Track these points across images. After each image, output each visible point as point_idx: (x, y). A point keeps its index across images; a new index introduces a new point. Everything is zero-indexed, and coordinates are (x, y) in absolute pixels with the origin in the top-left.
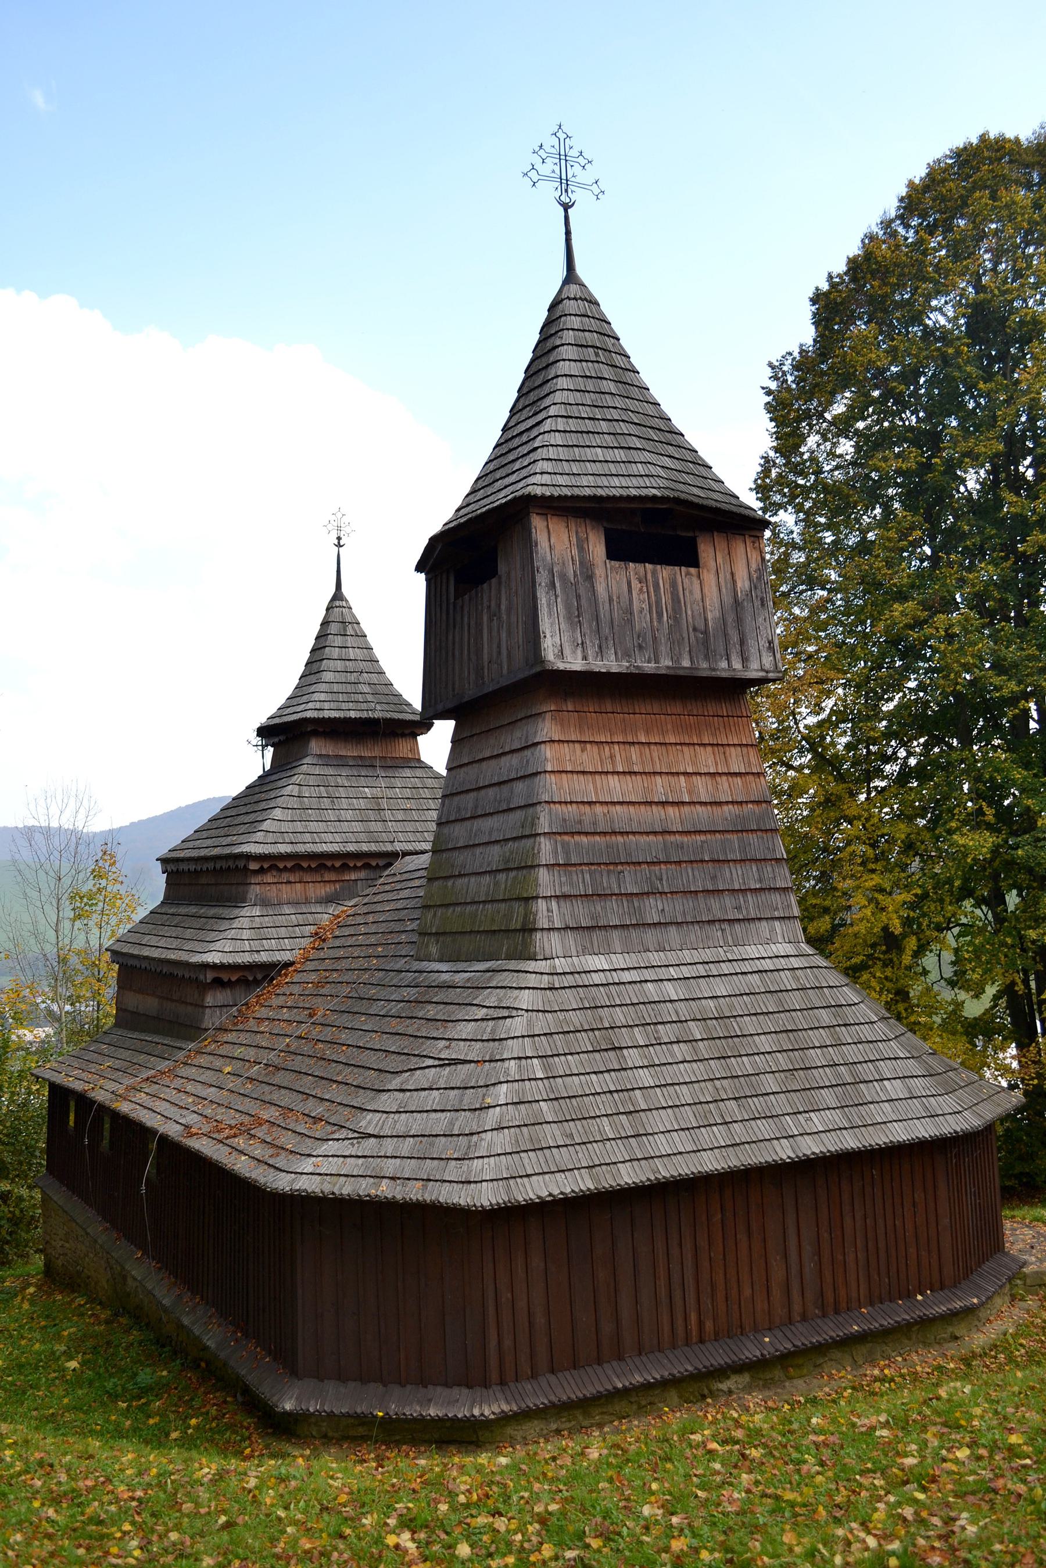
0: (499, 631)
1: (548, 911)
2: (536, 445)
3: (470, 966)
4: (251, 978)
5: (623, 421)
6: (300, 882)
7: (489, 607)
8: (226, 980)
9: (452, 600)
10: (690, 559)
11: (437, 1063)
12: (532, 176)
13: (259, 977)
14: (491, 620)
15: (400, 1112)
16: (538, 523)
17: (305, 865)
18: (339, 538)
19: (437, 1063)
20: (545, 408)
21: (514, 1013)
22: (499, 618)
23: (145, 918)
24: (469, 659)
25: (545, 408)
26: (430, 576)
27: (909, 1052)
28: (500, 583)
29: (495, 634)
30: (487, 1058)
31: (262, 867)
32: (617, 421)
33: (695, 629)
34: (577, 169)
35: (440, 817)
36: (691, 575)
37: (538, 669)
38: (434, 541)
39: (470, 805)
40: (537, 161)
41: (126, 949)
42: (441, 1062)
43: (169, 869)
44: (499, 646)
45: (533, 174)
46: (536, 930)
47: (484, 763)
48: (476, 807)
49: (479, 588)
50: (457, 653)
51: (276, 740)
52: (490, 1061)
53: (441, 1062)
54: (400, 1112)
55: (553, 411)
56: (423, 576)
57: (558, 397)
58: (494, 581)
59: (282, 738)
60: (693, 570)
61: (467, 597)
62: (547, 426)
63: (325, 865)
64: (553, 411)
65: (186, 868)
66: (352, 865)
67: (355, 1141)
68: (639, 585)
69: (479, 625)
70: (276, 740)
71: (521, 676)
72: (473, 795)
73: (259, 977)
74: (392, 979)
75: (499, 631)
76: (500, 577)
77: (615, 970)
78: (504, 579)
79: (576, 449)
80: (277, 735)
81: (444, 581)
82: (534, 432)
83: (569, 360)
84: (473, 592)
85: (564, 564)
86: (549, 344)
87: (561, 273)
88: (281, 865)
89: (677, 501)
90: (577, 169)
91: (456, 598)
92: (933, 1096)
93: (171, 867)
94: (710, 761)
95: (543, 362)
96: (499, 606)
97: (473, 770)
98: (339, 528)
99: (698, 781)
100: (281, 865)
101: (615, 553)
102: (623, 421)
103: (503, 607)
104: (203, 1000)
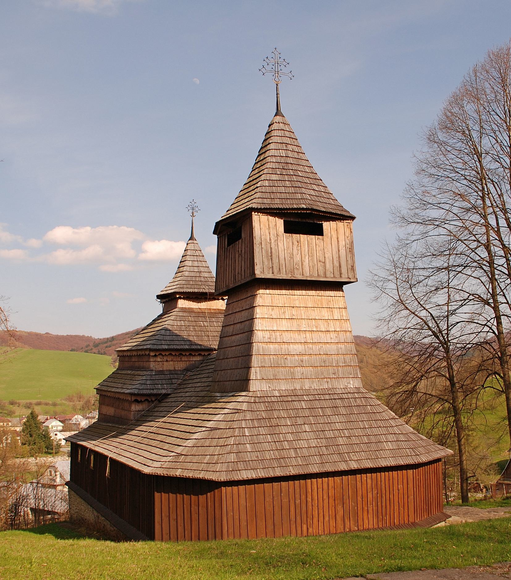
0: (241, 262)
1: (255, 373)
2: (258, 186)
3: (229, 394)
4: (150, 400)
5: (294, 175)
6: (172, 361)
7: (238, 251)
8: (140, 400)
9: (226, 247)
10: (318, 231)
11: (209, 429)
12: (262, 71)
13: (153, 399)
14: (239, 257)
15: (194, 447)
16: (256, 217)
17: (174, 354)
18: (193, 213)
19: (209, 429)
20: (263, 170)
21: (239, 411)
22: (242, 256)
23: (110, 376)
24: (231, 272)
25: (263, 170)
26: (219, 236)
27: (401, 431)
28: (242, 242)
29: (240, 262)
30: (228, 428)
31: (156, 354)
32: (292, 175)
33: (320, 261)
34: (282, 67)
35: (221, 335)
36: (320, 239)
37: (253, 278)
38: (217, 224)
39: (231, 331)
40: (265, 64)
41: (104, 388)
42: (211, 429)
43: (120, 355)
44: (241, 267)
45: (263, 70)
46: (250, 380)
47: (237, 314)
48: (233, 331)
49: (235, 243)
50: (227, 269)
51: (165, 300)
52: (229, 429)
53: (211, 429)
54: (194, 447)
55: (265, 171)
56: (216, 236)
57: (268, 165)
58: (240, 241)
59: (167, 300)
60: (320, 237)
61: (231, 246)
62: (263, 178)
63: (172, 354)
64: (265, 171)
65: (126, 354)
66: (193, 354)
67: (177, 457)
68: (297, 244)
69: (235, 257)
70: (165, 300)
71: (248, 280)
72: (232, 326)
73: (153, 399)
74: (194, 399)
75: (241, 262)
76: (242, 240)
77: (281, 396)
78: (243, 240)
79: (274, 187)
80: (164, 299)
81: (224, 237)
82: (258, 180)
83: (274, 149)
84: (233, 245)
85: (266, 235)
86: (267, 142)
87: (275, 111)
88: (164, 354)
89: (312, 210)
90: (282, 67)
91: (228, 247)
92: (408, 448)
93: (121, 354)
94: (326, 314)
95: (264, 151)
96: (242, 251)
97: (232, 317)
98: (193, 209)
99: (320, 322)
100: (164, 354)
101: (287, 231)
102: (294, 175)
103: (243, 252)
104: (131, 408)
